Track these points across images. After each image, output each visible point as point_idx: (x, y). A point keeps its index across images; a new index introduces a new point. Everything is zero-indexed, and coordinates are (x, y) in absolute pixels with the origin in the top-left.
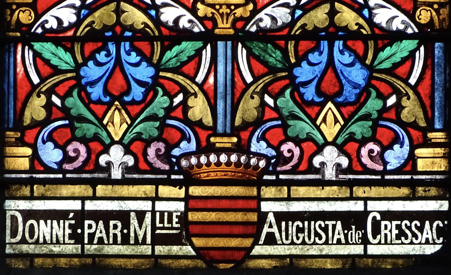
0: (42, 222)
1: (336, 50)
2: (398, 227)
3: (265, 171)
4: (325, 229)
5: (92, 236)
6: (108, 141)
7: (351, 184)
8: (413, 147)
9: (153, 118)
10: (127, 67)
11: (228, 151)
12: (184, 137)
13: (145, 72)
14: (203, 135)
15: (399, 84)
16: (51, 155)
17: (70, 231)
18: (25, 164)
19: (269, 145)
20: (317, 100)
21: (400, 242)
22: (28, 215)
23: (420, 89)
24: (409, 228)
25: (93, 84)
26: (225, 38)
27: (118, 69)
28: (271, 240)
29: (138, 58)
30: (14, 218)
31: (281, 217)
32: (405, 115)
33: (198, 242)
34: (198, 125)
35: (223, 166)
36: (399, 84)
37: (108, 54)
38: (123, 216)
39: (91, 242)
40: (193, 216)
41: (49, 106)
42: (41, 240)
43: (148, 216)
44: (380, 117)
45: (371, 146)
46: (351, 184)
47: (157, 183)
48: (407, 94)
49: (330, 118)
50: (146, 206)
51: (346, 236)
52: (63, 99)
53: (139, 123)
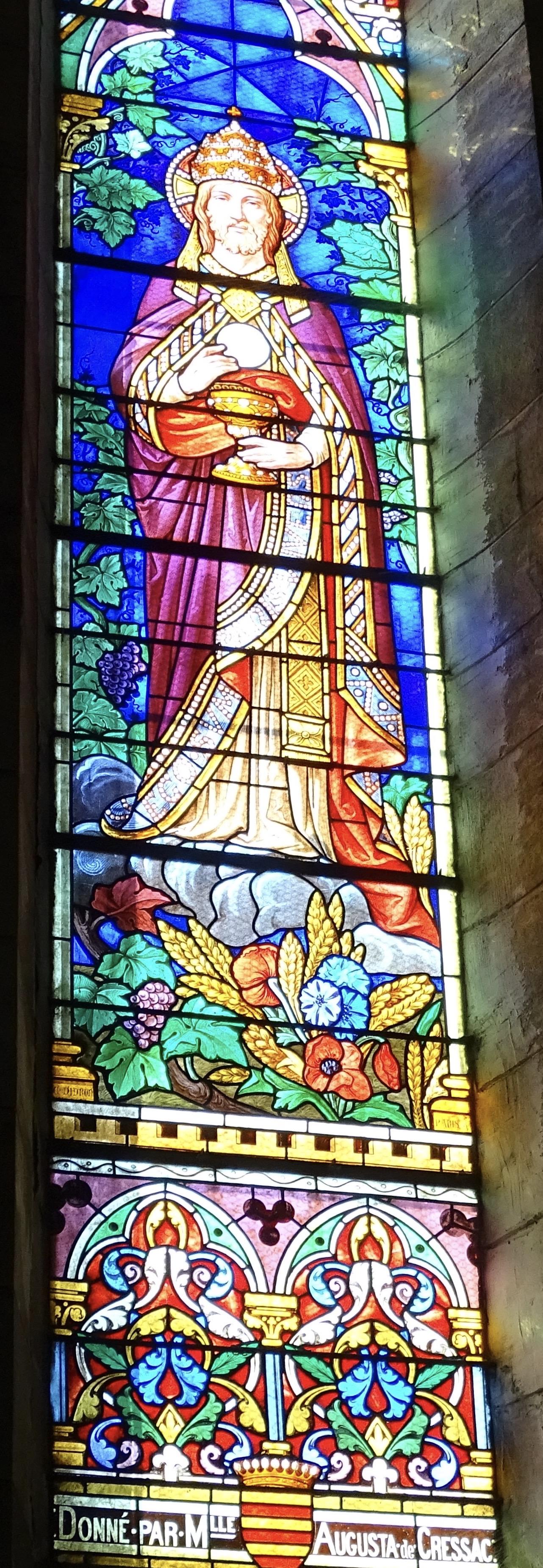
0: (96, 1520)
1: (379, 1369)
2: (449, 1544)
3: (316, 1480)
4: (378, 1541)
5: (147, 1538)
6: (371, 1456)
7: (403, 1498)
8: (459, 1466)
9: (412, 1435)
10: (384, 1385)
11: (280, 1457)
12: (237, 1442)
13: (198, 1378)
14: (256, 1440)
15: (238, 1391)
16: (104, 1452)
17: (125, 1530)
18: (79, 1459)
19: (321, 1455)
20: (366, 1413)
21: (449, 1558)
22: (82, 1511)
23: (256, 1394)
24: (459, 1545)
25: (145, 1384)
26: (273, 1350)
27: (375, 1385)
28: (325, 1550)
29: (395, 1377)
30: (67, 1515)
31: (334, 1527)
32: (245, 1421)
33: (255, 1549)
34: (249, 1431)
35: (284, 1472)
36: (238, 1391)
37: (367, 1371)
38: (180, 1519)
39: (146, 1542)
40: (247, 1523)
41: (313, 1418)
42: (95, 1538)
43: (203, 1521)
44: (219, 1421)
45: (211, 1449)
46: (403, 1498)
47: (211, 1487)
48: (450, 1415)
49: (378, 1434)
50: (201, 1510)
51: (399, 1550)
52: (115, 1397)
53: (194, 1426)
